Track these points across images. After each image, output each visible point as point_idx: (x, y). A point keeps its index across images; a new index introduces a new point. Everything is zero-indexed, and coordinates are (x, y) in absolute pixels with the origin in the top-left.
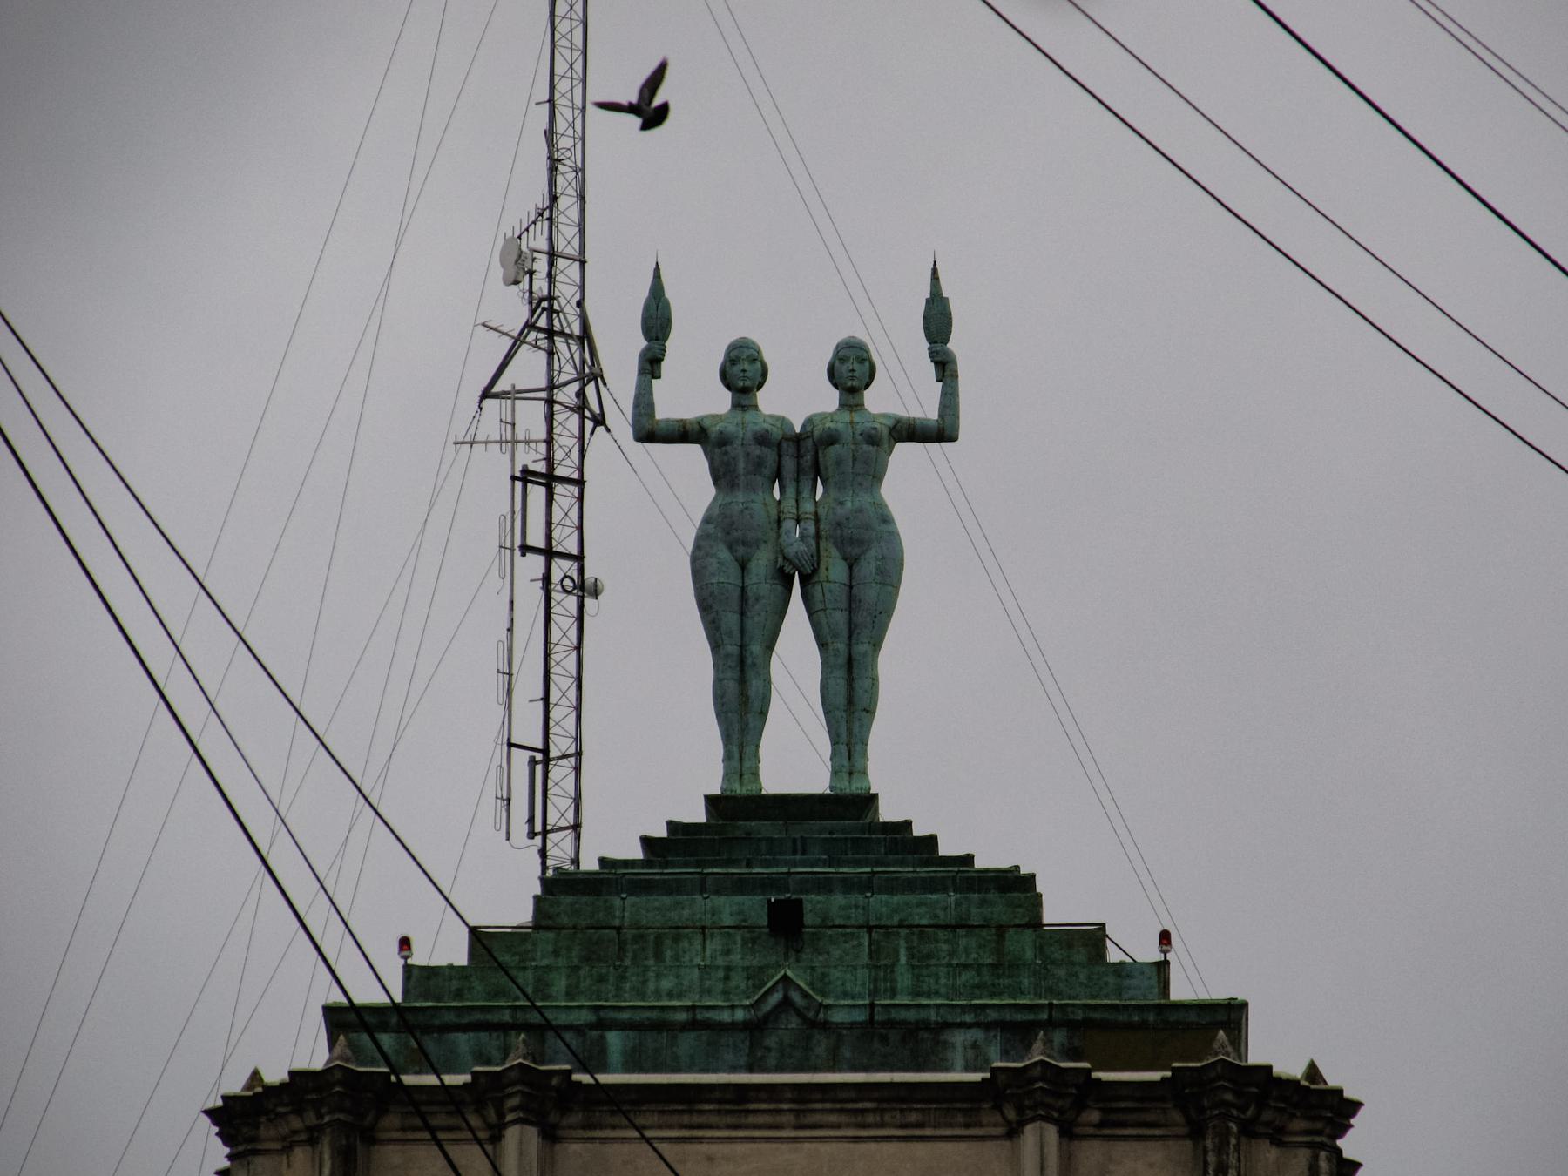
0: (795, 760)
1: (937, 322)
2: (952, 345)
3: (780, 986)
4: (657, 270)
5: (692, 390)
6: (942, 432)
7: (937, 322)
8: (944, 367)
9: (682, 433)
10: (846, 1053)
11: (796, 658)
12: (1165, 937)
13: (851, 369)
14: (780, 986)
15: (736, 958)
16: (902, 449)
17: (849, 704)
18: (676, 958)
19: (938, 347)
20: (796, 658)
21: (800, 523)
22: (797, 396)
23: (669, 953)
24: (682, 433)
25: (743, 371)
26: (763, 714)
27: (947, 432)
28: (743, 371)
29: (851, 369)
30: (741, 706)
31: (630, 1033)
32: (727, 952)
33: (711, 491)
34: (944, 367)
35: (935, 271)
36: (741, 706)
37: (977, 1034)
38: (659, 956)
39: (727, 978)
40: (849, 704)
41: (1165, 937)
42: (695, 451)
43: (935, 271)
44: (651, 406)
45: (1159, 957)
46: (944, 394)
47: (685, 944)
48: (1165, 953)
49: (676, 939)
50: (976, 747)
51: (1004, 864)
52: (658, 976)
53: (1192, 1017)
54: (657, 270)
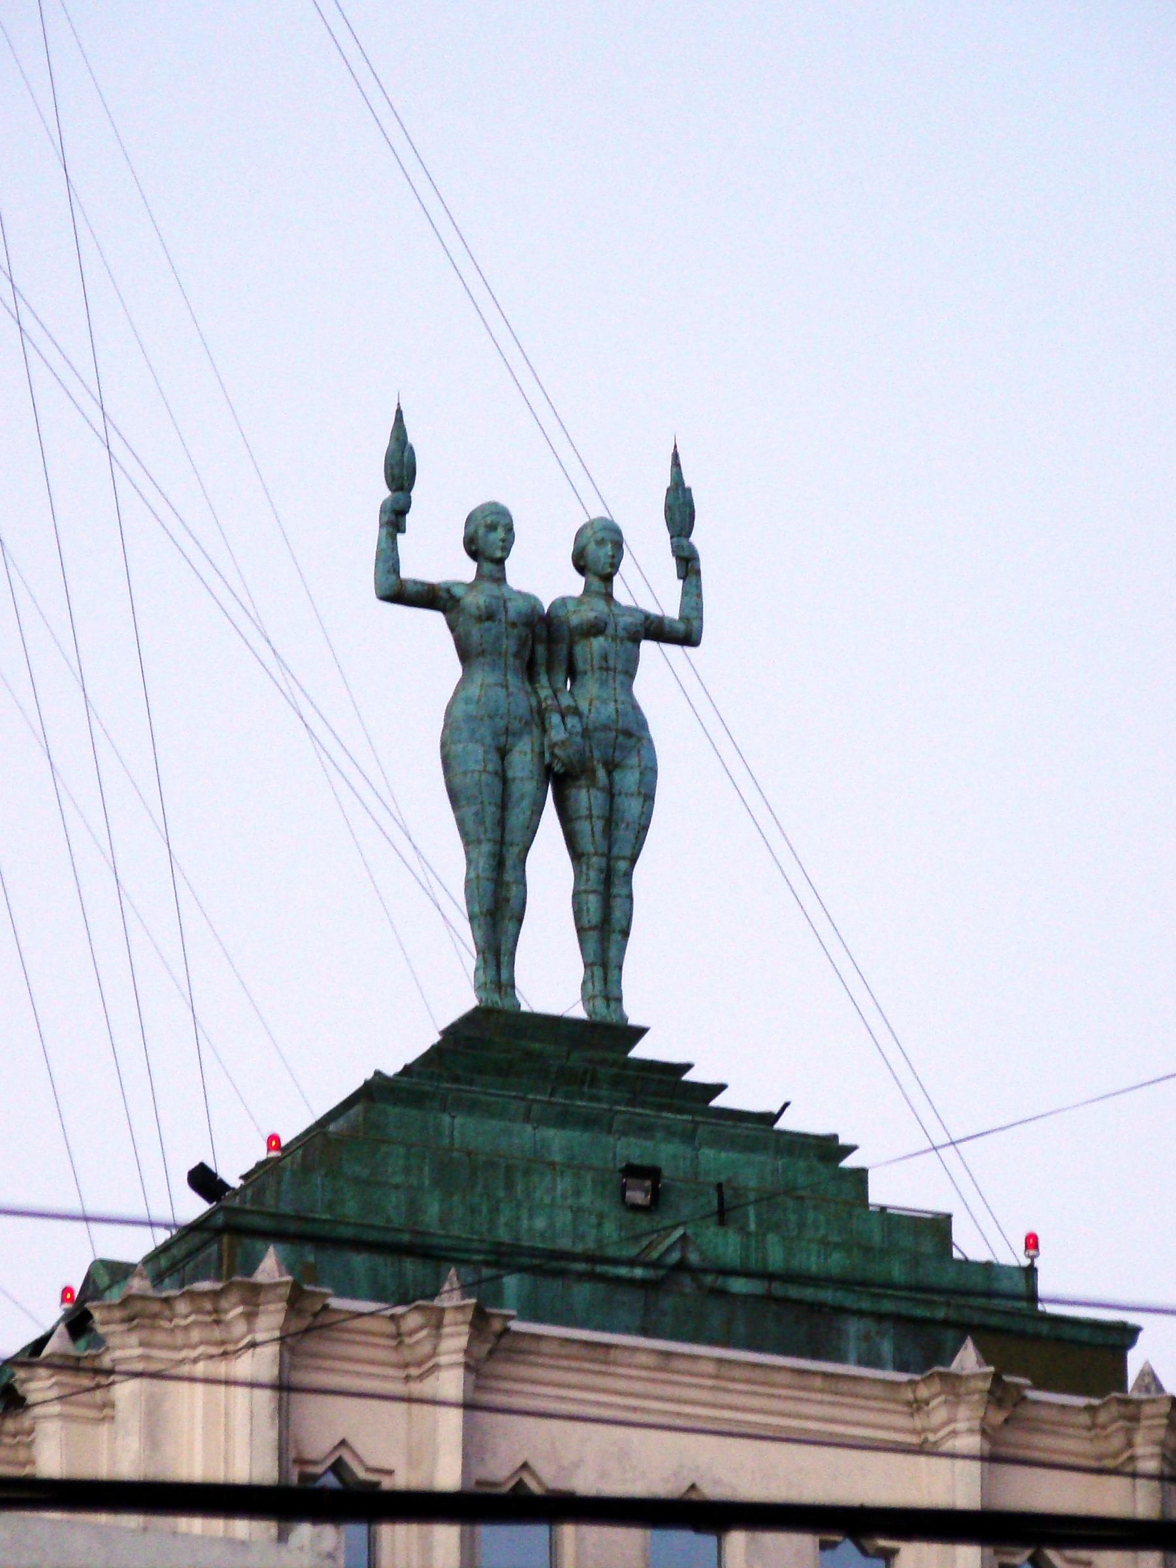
0: (549, 978)
1: (680, 512)
2: (695, 538)
3: (679, 1245)
4: (399, 412)
5: (435, 552)
6: (684, 634)
7: (680, 512)
8: (687, 565)
9: (428, 597)
10: (741, 1329)
11: (549, 869)
12: (1032, 1242)
13: (598, 554)
14: (679, 1245)
15: (586, 1200)
16: (648, 649)
17: (604, 927)
18: (528, 1194)
19: (684, 541)
20: (549, 869)
21: (551, 714)
22: (542, 574)
23: (520, 1188)
24: (428, 597)
25: (489, 538)
26: (626, 933)
27: (694, 637)
28: (489, 538)
29: (598, 554)
30: (497, 912)
31: (601, 1286)
32: (577, 1193)
33: (455, 670)
34: (687, 565)
35: (676, 456)
36: (497, 912)
37: (870, 1325)
38: (510, 1186)
39: (599, 1225)
40: (604, 927)
41: (1032, 1242)
42: (435, 620)
43: (676, 456)
44: (395, 569)
45: (1026, 1262)
46: (685, 593)
47: (535, 1178)
48: (1032, 1258)
49: (527, 1173)
50: (729, 994)
51: (361, 1083)
52: (531, 1217)
53: (1085, 1335)
54: (399, 412)
